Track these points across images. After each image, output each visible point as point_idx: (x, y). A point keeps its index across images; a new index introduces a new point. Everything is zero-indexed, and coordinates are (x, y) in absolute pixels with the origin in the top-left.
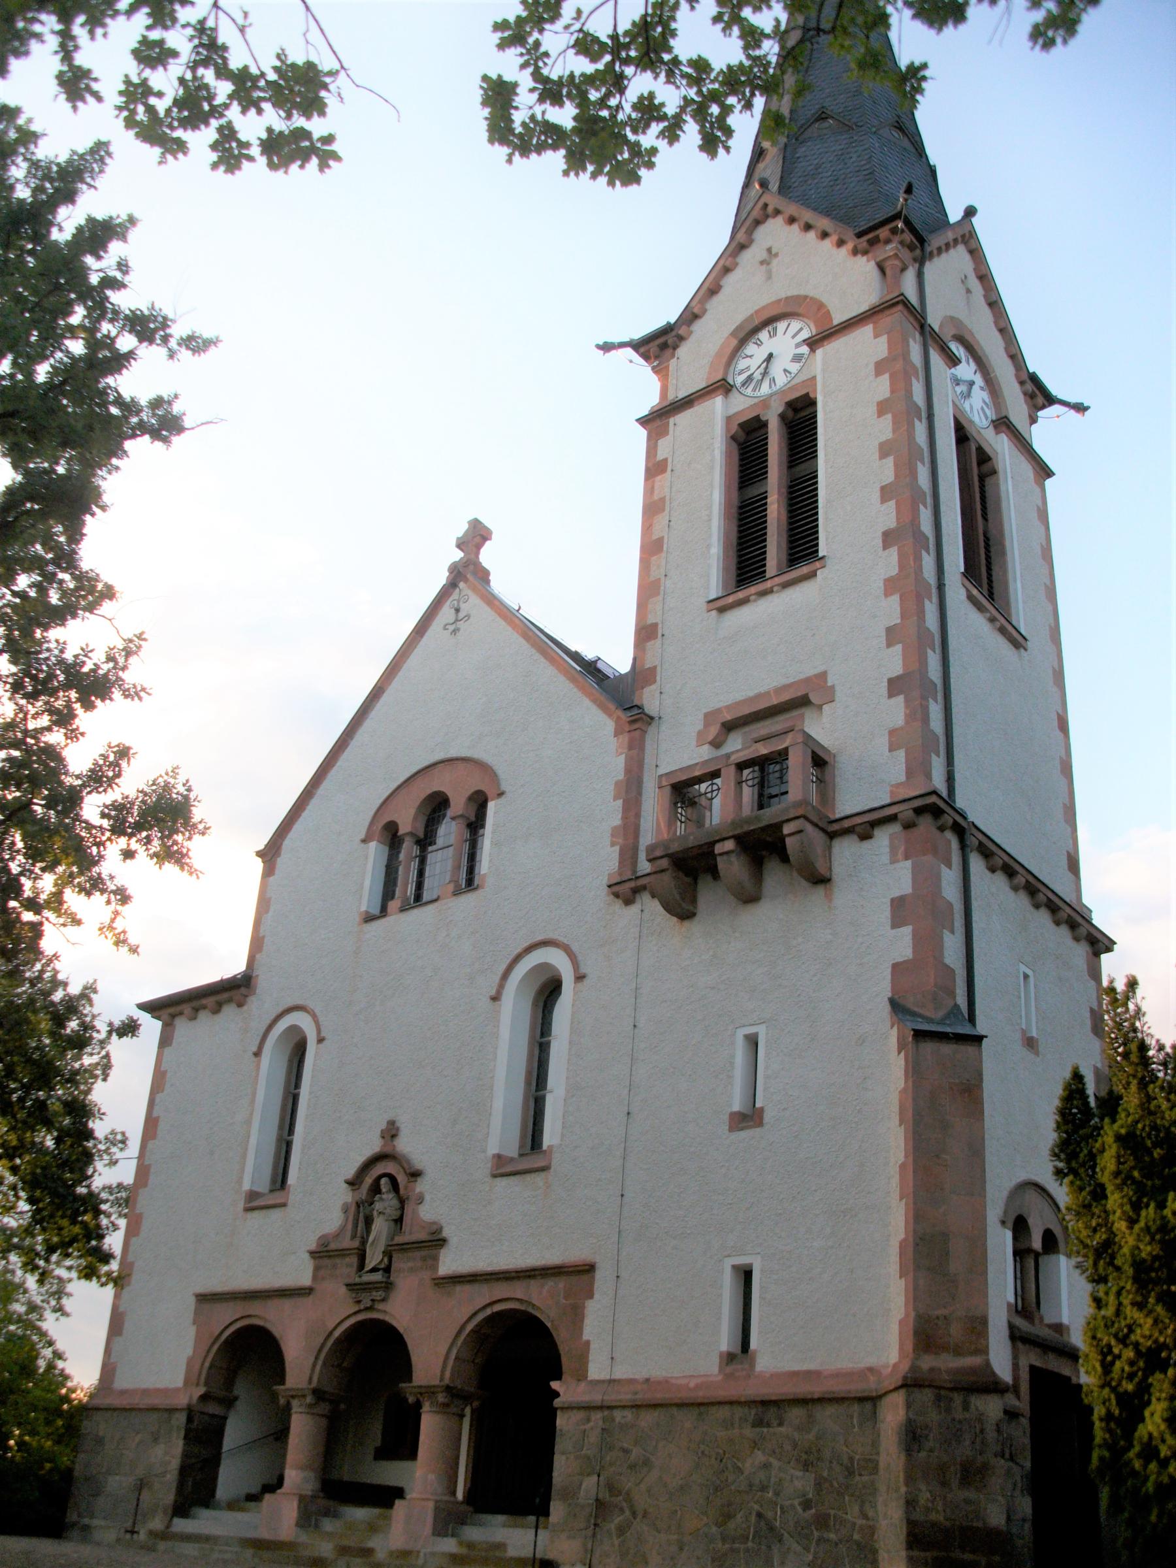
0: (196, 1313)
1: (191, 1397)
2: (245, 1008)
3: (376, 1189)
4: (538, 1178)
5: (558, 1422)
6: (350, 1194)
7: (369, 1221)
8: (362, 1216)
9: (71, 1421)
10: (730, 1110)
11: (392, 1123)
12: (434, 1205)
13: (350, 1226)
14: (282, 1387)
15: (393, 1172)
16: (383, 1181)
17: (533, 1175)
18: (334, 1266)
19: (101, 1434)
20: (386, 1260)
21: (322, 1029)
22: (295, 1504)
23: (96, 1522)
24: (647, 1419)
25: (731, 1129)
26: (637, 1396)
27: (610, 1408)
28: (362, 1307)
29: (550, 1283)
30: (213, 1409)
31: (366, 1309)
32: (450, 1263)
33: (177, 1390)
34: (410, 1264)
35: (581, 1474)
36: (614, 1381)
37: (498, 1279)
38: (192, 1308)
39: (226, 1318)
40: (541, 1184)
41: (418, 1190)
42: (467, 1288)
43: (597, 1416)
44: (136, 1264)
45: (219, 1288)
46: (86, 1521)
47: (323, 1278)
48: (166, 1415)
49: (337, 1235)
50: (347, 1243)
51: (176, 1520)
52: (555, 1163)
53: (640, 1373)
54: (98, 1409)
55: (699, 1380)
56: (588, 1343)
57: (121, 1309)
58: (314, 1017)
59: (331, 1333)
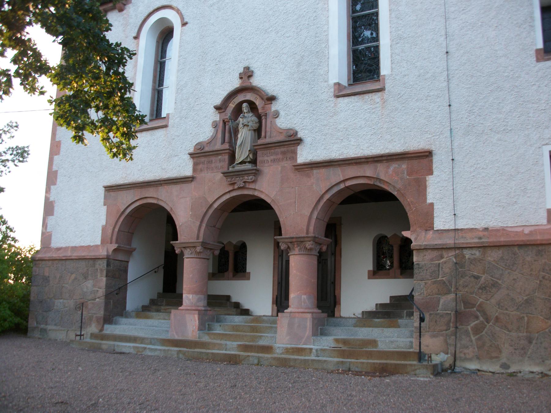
0: (106, 198)
1: (107, 251)
2: (124, 12)
3: (238, 111)
4: (376, 97)
5: (415, 259)
6: (218, 115)
7: (235, 131)
8: (228, 129)
9: (26, 266)
10: (535, 48)
11: (247, 69)
12: (287, 116)
13: (220, 135)
14: (177, 242)
15: (252, 99)
16: (245, 105)
17: (370, 95)
18: (210, 162)
19: (47, 274)
20: (251, 156)
21: (185, 17)
22: (196, 317)
23: (49, 327)
24: (493, 256)
25: (538, 60)
26: (483, 240)
27: (459, 248)
28: (236, 187)
29: (394, 166)
30: (121, 257)
31: (240, 188)
32: (304, 155)
33: (97, 246)
34: (272, 157)
36: (458, 230)
37: (349, 164)
38: (102, 196)
39: (127, 200)
40: (378, 100)
41: (273, 109)
42: (323, 171)
44: (59, 172)
45: (121, 182)
46: (42, 326)
47: (201, 170)
48: (91, 262)
49: (209, 143)
50: (218, 146)
51: (106, 326)
52: (387, 86)
53: (480, 224)
54: (42, 260)
55: (532, 229)
56: (432, 205)
57: (51, 199)
58: (178, 11)
59: (211, 205)
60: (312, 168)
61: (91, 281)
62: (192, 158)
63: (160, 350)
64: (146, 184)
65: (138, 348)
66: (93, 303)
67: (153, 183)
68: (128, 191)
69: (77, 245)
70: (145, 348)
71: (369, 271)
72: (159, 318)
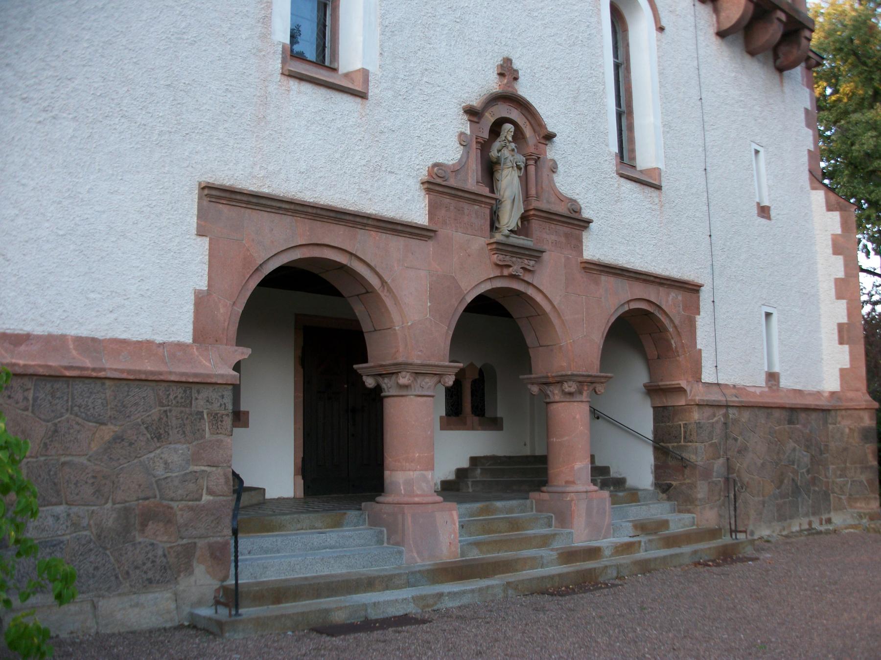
0: (202, 214)
3: (496, 129)
16: (508, 127)
24: (746, 415)
28: (506, 272)
35: (713, 459)
37: (637, 279)
39: (276, 243)
43: (723, 411)
45: (308, 197)
48: (179, 392)
60: (602, 271)
61: (182, 448)
62: (428, 190)
63: (473, 591)
64: (332, 214)
65: (423, 598)
66: (191, 509)
67: (351, 218)
68: (276, 218)
69: (99, 335)
70: (440, 595)
71: (441, 417)
72: (299, 526)
